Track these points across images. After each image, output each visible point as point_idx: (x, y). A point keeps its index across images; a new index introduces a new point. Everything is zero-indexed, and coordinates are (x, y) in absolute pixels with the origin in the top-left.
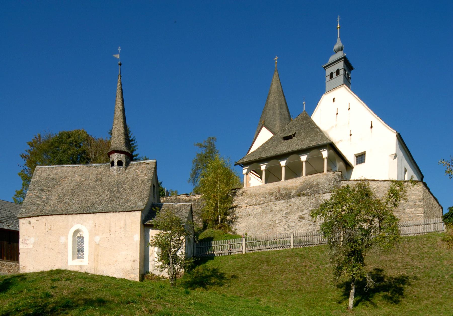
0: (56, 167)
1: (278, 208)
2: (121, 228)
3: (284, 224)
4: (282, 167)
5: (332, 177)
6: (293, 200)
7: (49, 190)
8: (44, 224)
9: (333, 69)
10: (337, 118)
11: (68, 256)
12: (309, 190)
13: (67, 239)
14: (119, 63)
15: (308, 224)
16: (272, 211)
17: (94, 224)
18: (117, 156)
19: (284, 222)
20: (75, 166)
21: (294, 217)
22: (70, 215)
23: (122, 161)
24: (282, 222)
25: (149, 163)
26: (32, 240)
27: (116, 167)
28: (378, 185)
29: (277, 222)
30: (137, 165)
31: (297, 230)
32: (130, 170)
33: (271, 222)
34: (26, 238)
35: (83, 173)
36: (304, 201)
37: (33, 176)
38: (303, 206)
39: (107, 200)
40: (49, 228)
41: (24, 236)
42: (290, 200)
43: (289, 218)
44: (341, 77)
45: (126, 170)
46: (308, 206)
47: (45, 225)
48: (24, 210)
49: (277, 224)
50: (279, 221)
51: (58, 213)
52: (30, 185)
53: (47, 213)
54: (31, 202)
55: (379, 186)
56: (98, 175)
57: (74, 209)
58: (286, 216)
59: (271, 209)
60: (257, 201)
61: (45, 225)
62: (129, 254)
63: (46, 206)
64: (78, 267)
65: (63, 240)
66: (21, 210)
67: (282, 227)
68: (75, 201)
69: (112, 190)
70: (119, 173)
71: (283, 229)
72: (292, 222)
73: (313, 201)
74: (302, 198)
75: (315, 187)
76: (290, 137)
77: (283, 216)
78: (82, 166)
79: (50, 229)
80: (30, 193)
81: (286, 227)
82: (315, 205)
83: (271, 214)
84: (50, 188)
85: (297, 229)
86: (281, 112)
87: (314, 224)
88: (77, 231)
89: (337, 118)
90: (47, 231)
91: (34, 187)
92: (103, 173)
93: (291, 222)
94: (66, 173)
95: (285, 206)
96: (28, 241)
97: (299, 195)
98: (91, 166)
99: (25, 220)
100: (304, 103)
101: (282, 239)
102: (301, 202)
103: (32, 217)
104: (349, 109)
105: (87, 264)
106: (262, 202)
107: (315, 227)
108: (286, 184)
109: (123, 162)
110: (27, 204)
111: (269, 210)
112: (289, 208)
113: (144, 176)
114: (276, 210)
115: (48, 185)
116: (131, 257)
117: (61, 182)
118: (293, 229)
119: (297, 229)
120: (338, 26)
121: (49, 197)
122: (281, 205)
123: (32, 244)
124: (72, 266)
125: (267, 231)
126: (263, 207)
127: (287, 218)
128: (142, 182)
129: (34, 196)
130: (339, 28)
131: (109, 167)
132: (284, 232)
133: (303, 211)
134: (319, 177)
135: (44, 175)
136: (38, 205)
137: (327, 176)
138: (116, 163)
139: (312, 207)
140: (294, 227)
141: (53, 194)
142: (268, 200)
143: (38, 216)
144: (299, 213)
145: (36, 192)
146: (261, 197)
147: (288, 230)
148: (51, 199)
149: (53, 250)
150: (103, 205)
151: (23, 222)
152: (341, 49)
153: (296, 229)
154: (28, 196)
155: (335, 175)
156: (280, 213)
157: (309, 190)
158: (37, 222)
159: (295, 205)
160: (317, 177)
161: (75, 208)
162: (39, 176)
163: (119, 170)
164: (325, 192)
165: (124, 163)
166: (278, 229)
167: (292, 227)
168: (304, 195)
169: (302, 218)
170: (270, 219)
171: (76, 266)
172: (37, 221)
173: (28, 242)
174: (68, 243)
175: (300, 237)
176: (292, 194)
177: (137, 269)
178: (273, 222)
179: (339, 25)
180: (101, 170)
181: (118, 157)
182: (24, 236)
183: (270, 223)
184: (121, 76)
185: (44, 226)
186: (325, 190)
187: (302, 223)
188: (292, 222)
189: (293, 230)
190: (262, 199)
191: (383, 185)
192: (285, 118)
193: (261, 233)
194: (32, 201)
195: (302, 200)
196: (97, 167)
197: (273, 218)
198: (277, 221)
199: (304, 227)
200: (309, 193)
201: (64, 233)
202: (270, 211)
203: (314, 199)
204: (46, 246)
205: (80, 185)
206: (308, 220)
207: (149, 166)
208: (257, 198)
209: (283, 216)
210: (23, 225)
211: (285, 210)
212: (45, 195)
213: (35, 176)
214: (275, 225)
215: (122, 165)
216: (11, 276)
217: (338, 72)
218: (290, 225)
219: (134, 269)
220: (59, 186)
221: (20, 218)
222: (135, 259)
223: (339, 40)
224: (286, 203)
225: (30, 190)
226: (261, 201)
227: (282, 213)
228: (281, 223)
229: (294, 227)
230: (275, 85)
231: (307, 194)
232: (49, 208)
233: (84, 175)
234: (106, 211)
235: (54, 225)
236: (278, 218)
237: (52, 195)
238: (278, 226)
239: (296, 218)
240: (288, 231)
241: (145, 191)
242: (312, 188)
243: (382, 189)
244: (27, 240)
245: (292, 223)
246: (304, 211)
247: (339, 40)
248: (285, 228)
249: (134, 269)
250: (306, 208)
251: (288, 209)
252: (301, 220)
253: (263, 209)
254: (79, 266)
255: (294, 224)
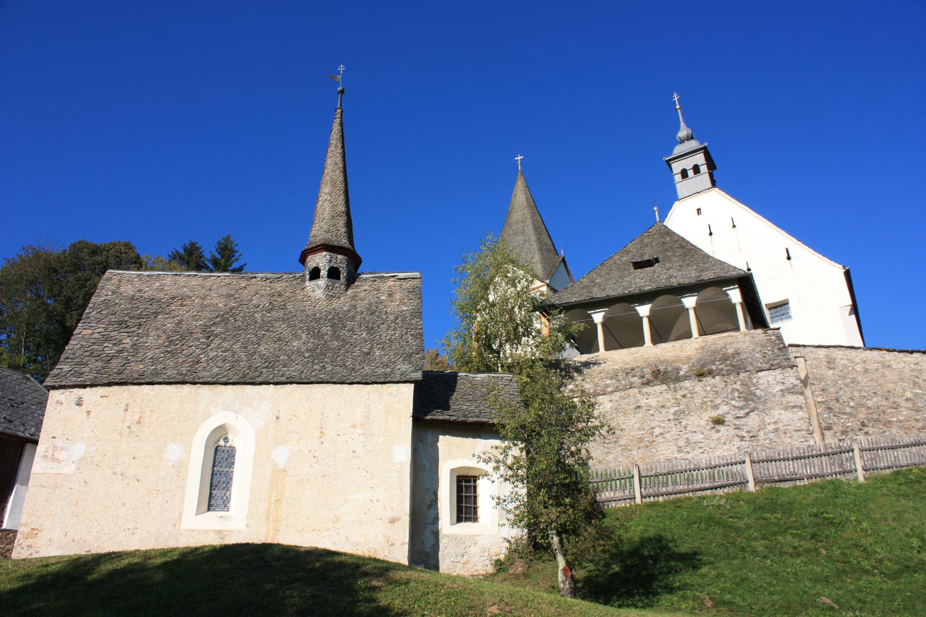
0: (159, 275)
1: (653, 402)
2: (354, 426)
3: (675, 437)
4: (642, 318)
5: (765, 340)
6: (687, 384)
7: (140, 324)
8: (124, 407)
9: (688, 163)
10: (711, 240)
11: (183, 499)
12: (720, 364)
13: (188, 452)
14: (340, 88)
15: (738, 436)
16: (639, 407)
17: (276, 413)
18: (328, 257)
19: (673, 433)
20: (211, 276)
21: (700, 420)
22: (205, 386)
23: (341, 269)
24: (669, 432)
25: (405, 279)
26: (78, 450)
27: (322, 282)
28: (862, 357)
29: (657, 431)
30: (375, 281)
31: (711, 450)
32: (359, 290)
33: (640, 433)
34: (58, 443)
35: (233, 292)
36: (716, 387)
37: (97, 291)
38: (715, 398)
39: (307, 355)
40: (137, 418)
41: (54, 438)
42: (682, 384)
43: (684, 423)
44: (704, 177)
45: (347, 290)
46: (727, 397)
47: (126, 410)
48: (67, 368)
49: (657, 436)
50: (662, 430)
51: (169, 379)
52: (87, 311)
53: (137, 379)
54: (88, 349)
55: (864, 359)
56: (275, 298)
57: (214, 371)
58: (678, 419)
59: (637, 405)
60: (596, 385)
61: (126, 410)
62: (378, 501)
63: (133, 362)
64: (211, 533)
65: (173, 452)
66: (57, 367)
67: (671, 444)
68: (215, 354)
69: (316, 331)
70: (332, 296)
71: (675, 448)
72: (695, 432)
73: (738, 386)
74: (709, 380)
75: (733, 358)
76: (649, 263)
77: (669, 420)
78: (229, 276)
79: (139, 422)
80: (86, 327)
81: (681, 443)
82: (744, 395)
83: (638, 416)
84: (145, 320)
85: (711, 448)
86: (539, 239)
87: (751, 437)
88: (221, 432)
89: (711, 240)
90: (129, 427)
91: (98, 316)
92: (288, 294)
93: (693, 432)
94: (185, 289)
95: (671, 397)
96: (63, 452)
97: (700, 375)
98: (253, 278)
99: (68, 392)
100: (655, 208)
101: (724, 468)
102: (708, 389)
103: (92, 386)
104: (734, 226)
105: (243, 527)
106: (610, 389)
107: (754, 444)
108: (660, 352)
109: (342, 272)
110: (77, 354)
111: (633, 407)
112: (682, 403)
113: (398, 305)
114: (650, 406)
115: (138, 312)
116: (384, 508)
117: (173, 308)
118: (701, 448)
119: (711, 448)
120: (678, 107)
121: (141, 340)
122: (658, 393)
123: (74, 462)
124: (193, 531)
125: (634, 452)
126: (616, 398)
127: (680, 423)
128: (397, 318)
129: (96, 335)
130: (680, 109)
131: (304, 281)
132: (679, 456)
133: (717, 409)
134: (734, 338)
135: (128, 290)
136: (109, 358)
137: (753, 337)
138: (324, 273)
139: (737, 399)
140: (700, 442)
141: (152, 334)
142: (625, 385)
143: (109, 384)
144: (708, 412)
145: (104, 326)
146: (606, 378)
147: (688, 450)
148: (146, 345)
149: (138, 480)
150: (296, 366)
151: (59, 399)
152: (690, 138)
153: (708, 449)
154: (80, 336)
155: (769, 336)
156: (661, 412)
157: (720, 364)
158: (104, 400)
159: (695, 395)
160: (730, 340)
161: (216, 370)
162: (114, 292)
163: (331, 288)
164: (760, 367)
165: (343, 274)
166: (663, 448)
167: (696, 443)
168: (710, 373)
169: (719, 421)
170: (637, 426)
171: (206, 531)
172: (101, 397)
173: (62, 455)
174: (189, 462)
175: (730, 466)
176: (682, 373)
177: (403, 544)
178: (645, 432)
179: (679, 104)
180: (279, 286)
181: (331, 261)
182: (54, 438)
183: (639, 435)
184: (342, 111)
185: (122, 413)
186: (759, 365)
187: (720, 434)
188: (695, 432)
189: (701, 450)
190: (609, 382)
191: (873, 357)
192: (548, 250)
193: (618, 457)
194: (91, 348)
195: (710, 385)
196: (268, 281)
197: (646, 424)
198: (655, 430)
199: (727, 442)
200: (722, 369)
201: (181, 434)
202: (636, 408)
203: (739, 383)
204: (119, 470)
205: (224, 318)
206: (736, 429)
207: (407, 285)
208: (597, 379)
209: (669, 420)
210: (59, 407)
211: (673, 406)
212: (130, 334)
213: (101, 290)
214: (653, 439)
215: (339, 278)
216: (180, 554)
217: (696, 169)
218: (690, 438)
219: (392, 545)
220: (167, 316)
221: (54, 388)
222: (395, 515)
223: (682, 124)
224: (672, 390)
225: (86, 321)
226: (607, 386)
227: (667, 412)
228: (667, 436)
229: (700, 442)
230: (520, 196)
231: (719, 373)
232: (141, 366)
233: (237, 296)
234: (313, 379)
235: (152, 411)
236: (658, 423)
237: (147, 335)
238: (661, 441)
239: (703, 423)
240: (688, 452)
241: (410, 337)
242: (728, 360)
243: (872, 365)
244: (62, 449)
245: (694, 434)
246: (721, 408)
247: (682, 124)
248: (680, 447)
249: (392, 545)
250: (724, 401)
251: (679, 404)
252: (718, 427)
253: (617, 404)
254: (215, 531)
255: (701, 436)
